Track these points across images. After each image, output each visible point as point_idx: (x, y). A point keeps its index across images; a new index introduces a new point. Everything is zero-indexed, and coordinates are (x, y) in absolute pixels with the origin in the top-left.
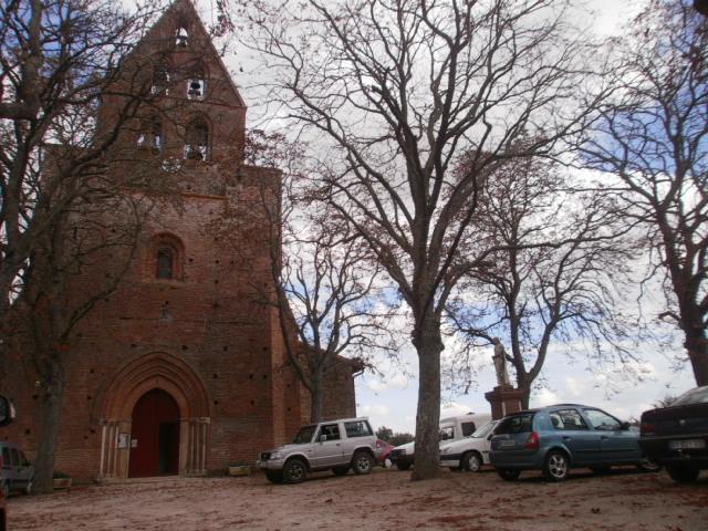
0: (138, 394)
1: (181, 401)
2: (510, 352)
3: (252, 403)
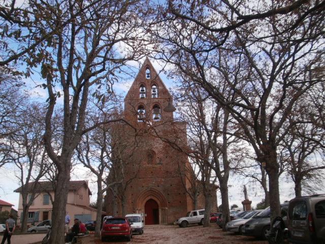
0: (145, 201)
1: (159, 202)
2: (222, 58)
3: (180, 202)
